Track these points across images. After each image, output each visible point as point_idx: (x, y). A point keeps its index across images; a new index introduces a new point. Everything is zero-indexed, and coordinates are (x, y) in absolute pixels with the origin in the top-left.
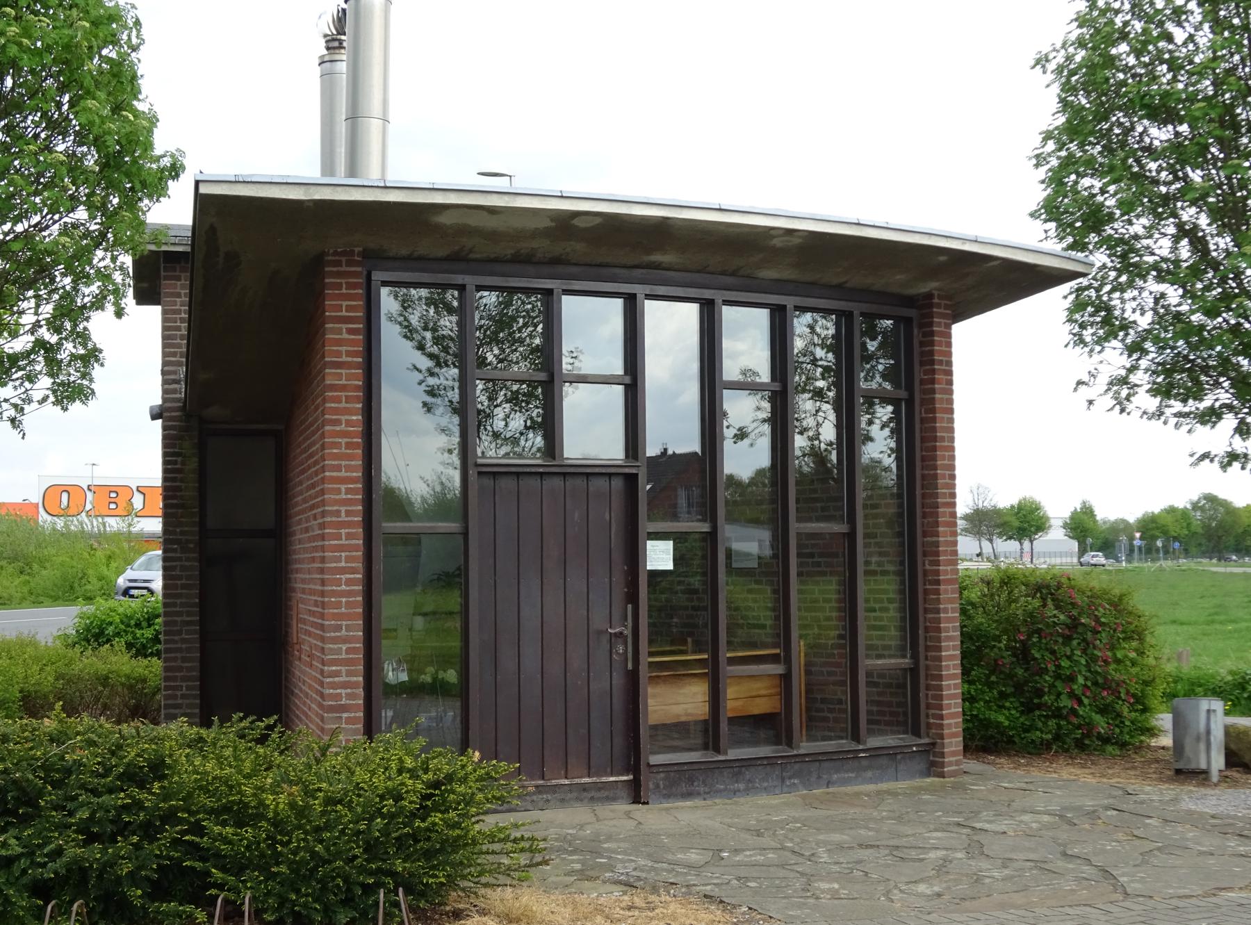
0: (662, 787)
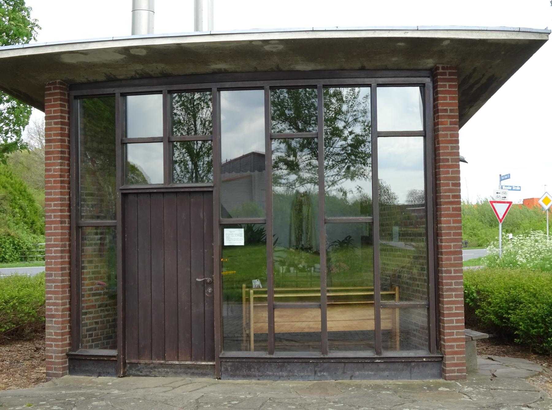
0: (229, 370)
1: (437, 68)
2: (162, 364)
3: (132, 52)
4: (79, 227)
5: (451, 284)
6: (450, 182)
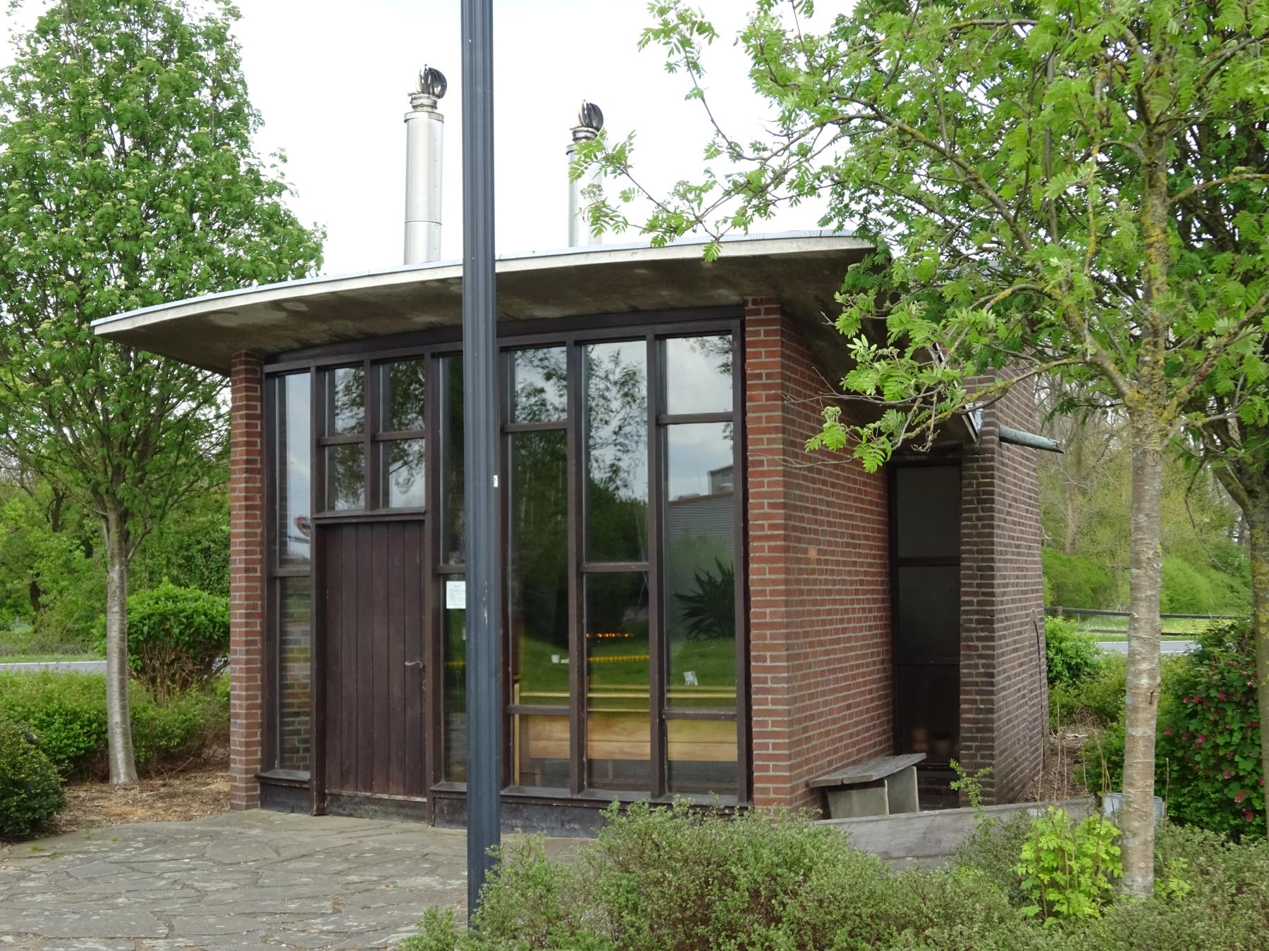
1: (745, 303)
2: (368, 798)
3: (287, 305)
4: (275, 578)
5: (765, 680)
6: (766, 501)
